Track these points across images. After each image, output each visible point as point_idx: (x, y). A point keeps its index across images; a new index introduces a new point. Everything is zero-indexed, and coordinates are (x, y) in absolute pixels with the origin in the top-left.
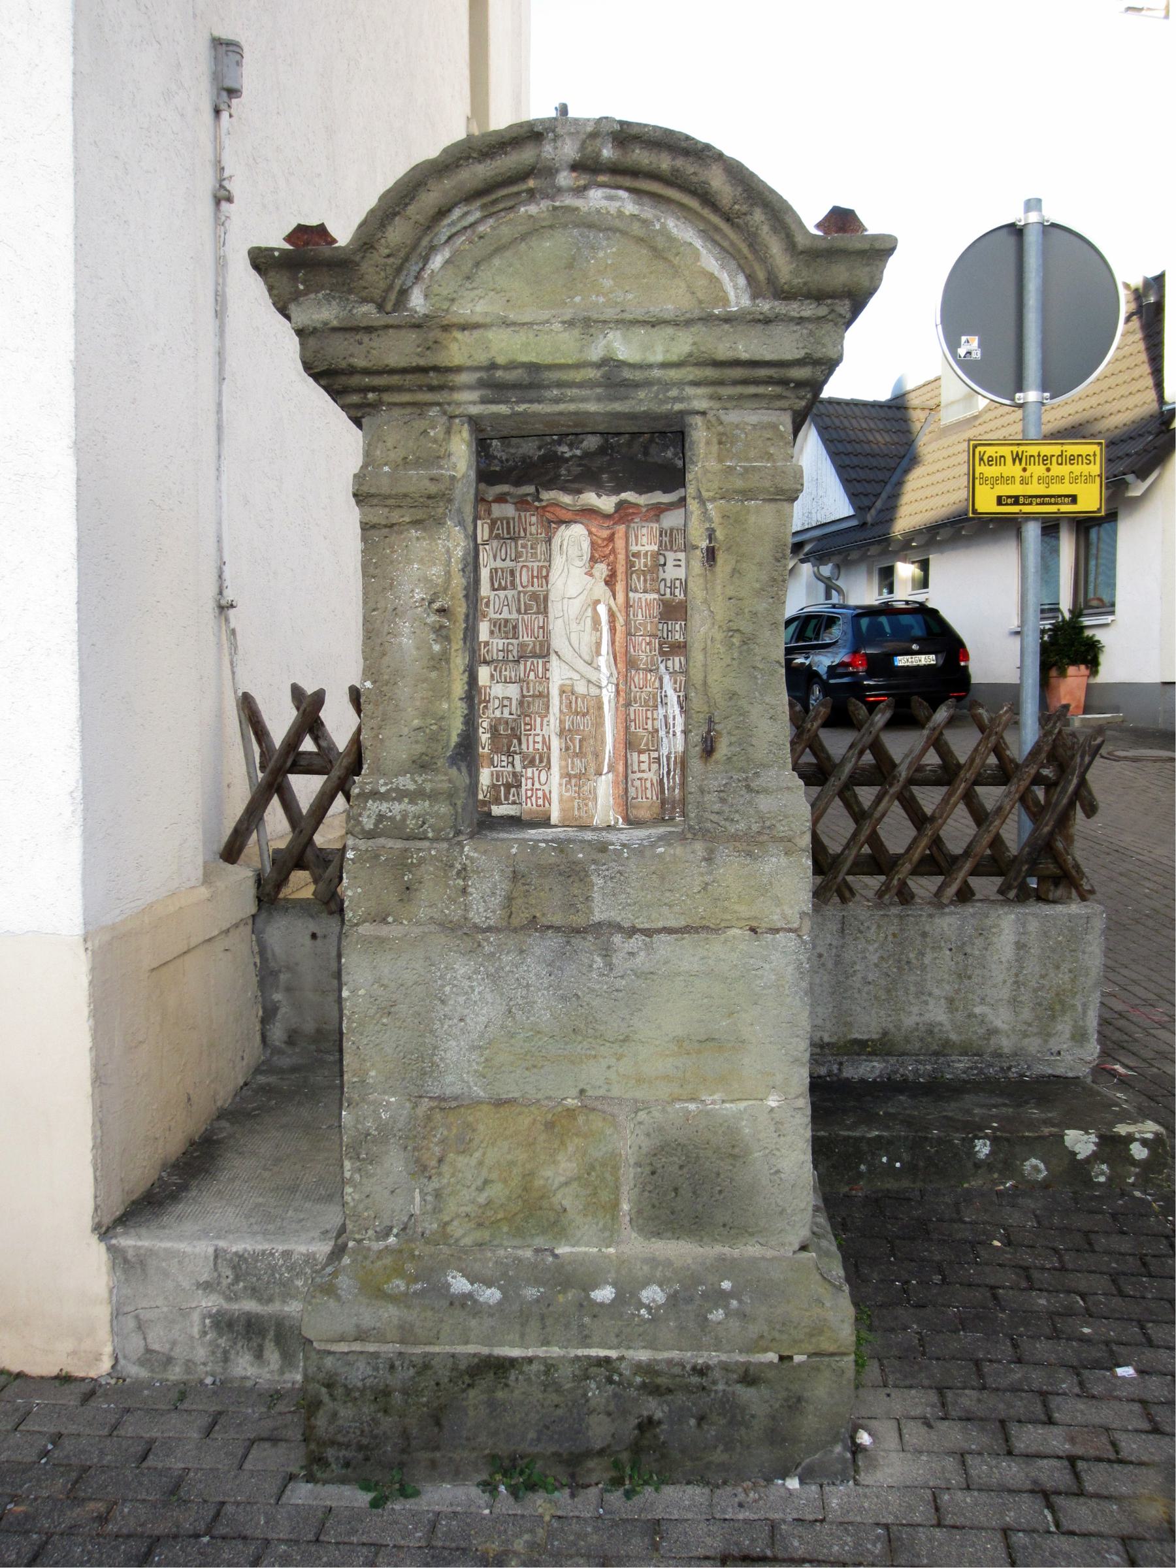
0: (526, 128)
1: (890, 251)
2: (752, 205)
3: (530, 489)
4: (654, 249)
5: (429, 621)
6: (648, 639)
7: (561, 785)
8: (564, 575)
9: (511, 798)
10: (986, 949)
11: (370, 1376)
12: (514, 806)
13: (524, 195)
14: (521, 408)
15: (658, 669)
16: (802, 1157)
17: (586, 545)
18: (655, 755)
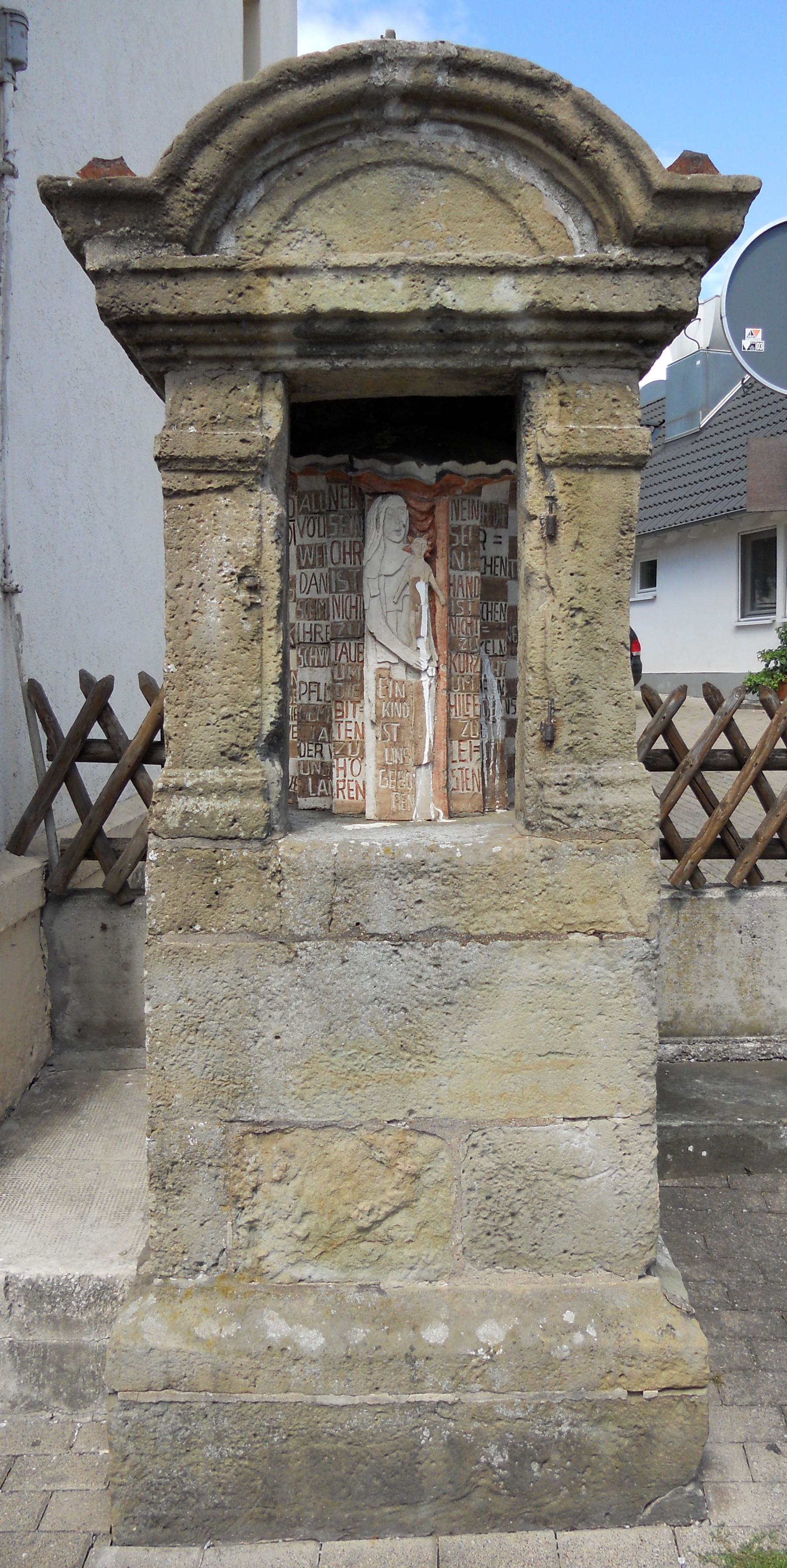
1: (752, 195)
3: (345, 458)
4: (491, 190)
5: (239, 597)
6: (469, 619)
7: (377, 776)
8: (381, 550)
9: (320, 790)
11: (180, 1429)
12: (323, 799)
13: (348, 127)
14: (341, 364)
16: (649, 1177)
17: (404, 517)
18: (478, 743)
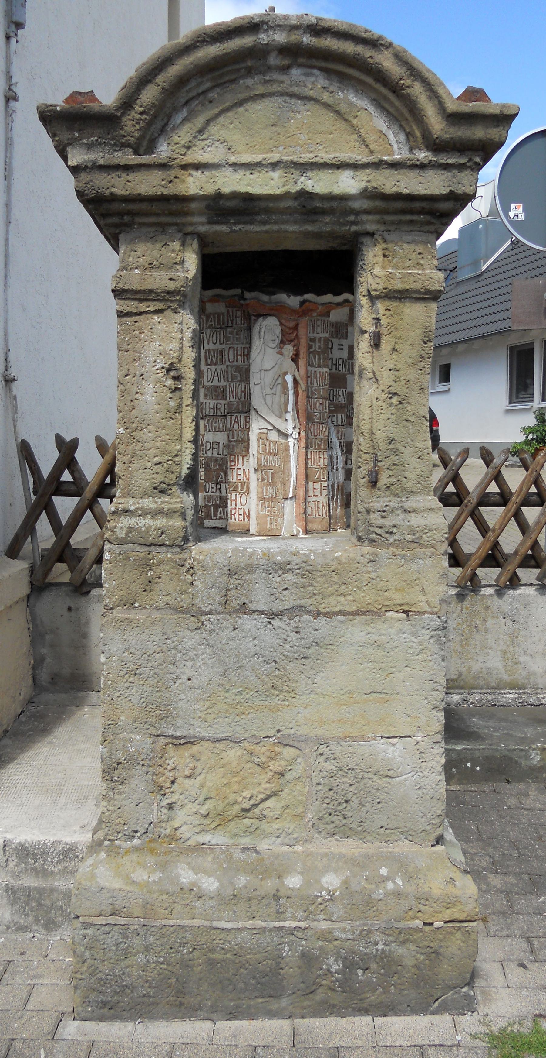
0: (247, 21)
1: (512, 117)
2: (413, 81)
6: (321, 400)
7: (258, 505)
9: (219, 515)
10: (528, 618)
11: (121, 942)
12: (221, 521)
13: (243, 71)
15: (327, 422)
16: (439, 778)
17: (278, 331)
